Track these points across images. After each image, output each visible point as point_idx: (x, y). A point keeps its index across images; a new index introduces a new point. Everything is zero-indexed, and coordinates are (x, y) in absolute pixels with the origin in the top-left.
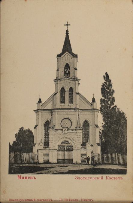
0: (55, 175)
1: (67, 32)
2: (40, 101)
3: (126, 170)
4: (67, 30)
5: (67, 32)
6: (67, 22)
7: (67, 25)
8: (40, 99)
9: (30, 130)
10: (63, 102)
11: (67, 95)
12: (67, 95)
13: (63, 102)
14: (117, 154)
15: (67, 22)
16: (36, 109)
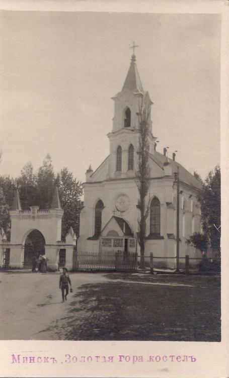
1: (133, 59)
5: (133, 59)
10: (119, 168)
13: (119, 168)
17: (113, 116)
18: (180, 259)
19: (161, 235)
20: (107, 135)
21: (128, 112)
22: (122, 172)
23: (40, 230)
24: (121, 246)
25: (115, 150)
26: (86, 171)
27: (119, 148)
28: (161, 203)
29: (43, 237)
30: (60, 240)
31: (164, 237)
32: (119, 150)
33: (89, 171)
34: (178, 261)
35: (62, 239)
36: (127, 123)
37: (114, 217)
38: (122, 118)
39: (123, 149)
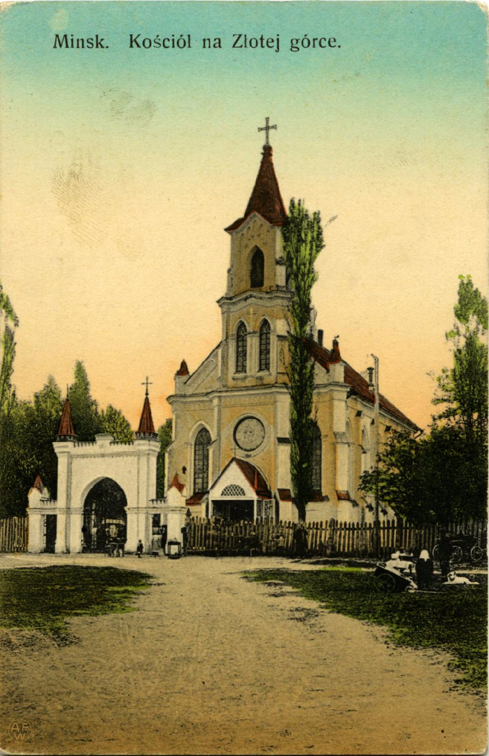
0: (409, 416)
1: (267, 151)
2: (183, 369)
3: (487, 575)
4: (268, 142)
5: (267, 151)
6: (267, 119)
7: (267, 128)
8: (184, 365)
9: (321, 216)
10: (241, 367)
11: (253, 344)
12: (253, 344)
13: (241, 367)
14: (346, 550)
15: (267, 119)
16: (172, 393)
17: (227, 266)
18: (136, 458)
19: (324, 495)
20: (218, 302)
21: (257, 258)
22: (248, 373)
23: (118, 482)
24: (88, 547)
25: (233, 331)
26: (176, 372)
27: (242, 325)
28: (323, 434)
29: (121, 490)
30: (154, 497)
31: (329, 497)
32: (241, 335)
33: (183, 369)
34: (338, 529)
35: (158, 497)
36: (257, 279)
37: (233, 459)
38: (245, 269)
39: (249, 329)
